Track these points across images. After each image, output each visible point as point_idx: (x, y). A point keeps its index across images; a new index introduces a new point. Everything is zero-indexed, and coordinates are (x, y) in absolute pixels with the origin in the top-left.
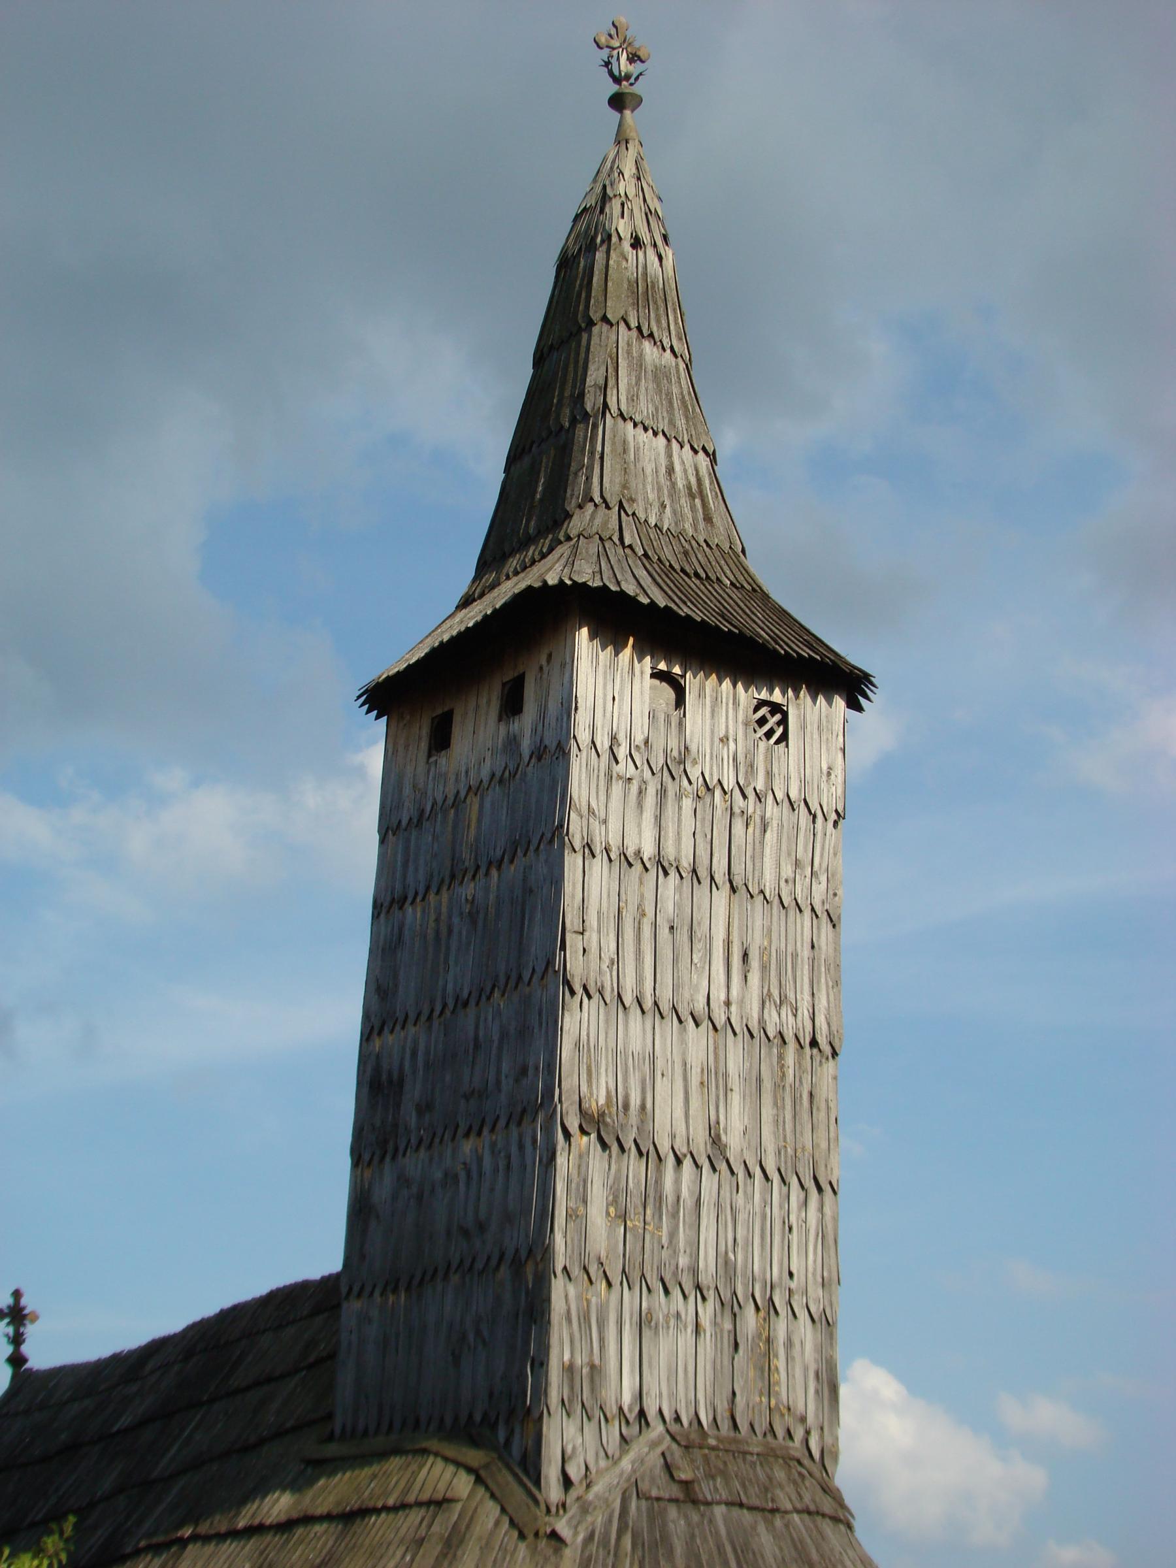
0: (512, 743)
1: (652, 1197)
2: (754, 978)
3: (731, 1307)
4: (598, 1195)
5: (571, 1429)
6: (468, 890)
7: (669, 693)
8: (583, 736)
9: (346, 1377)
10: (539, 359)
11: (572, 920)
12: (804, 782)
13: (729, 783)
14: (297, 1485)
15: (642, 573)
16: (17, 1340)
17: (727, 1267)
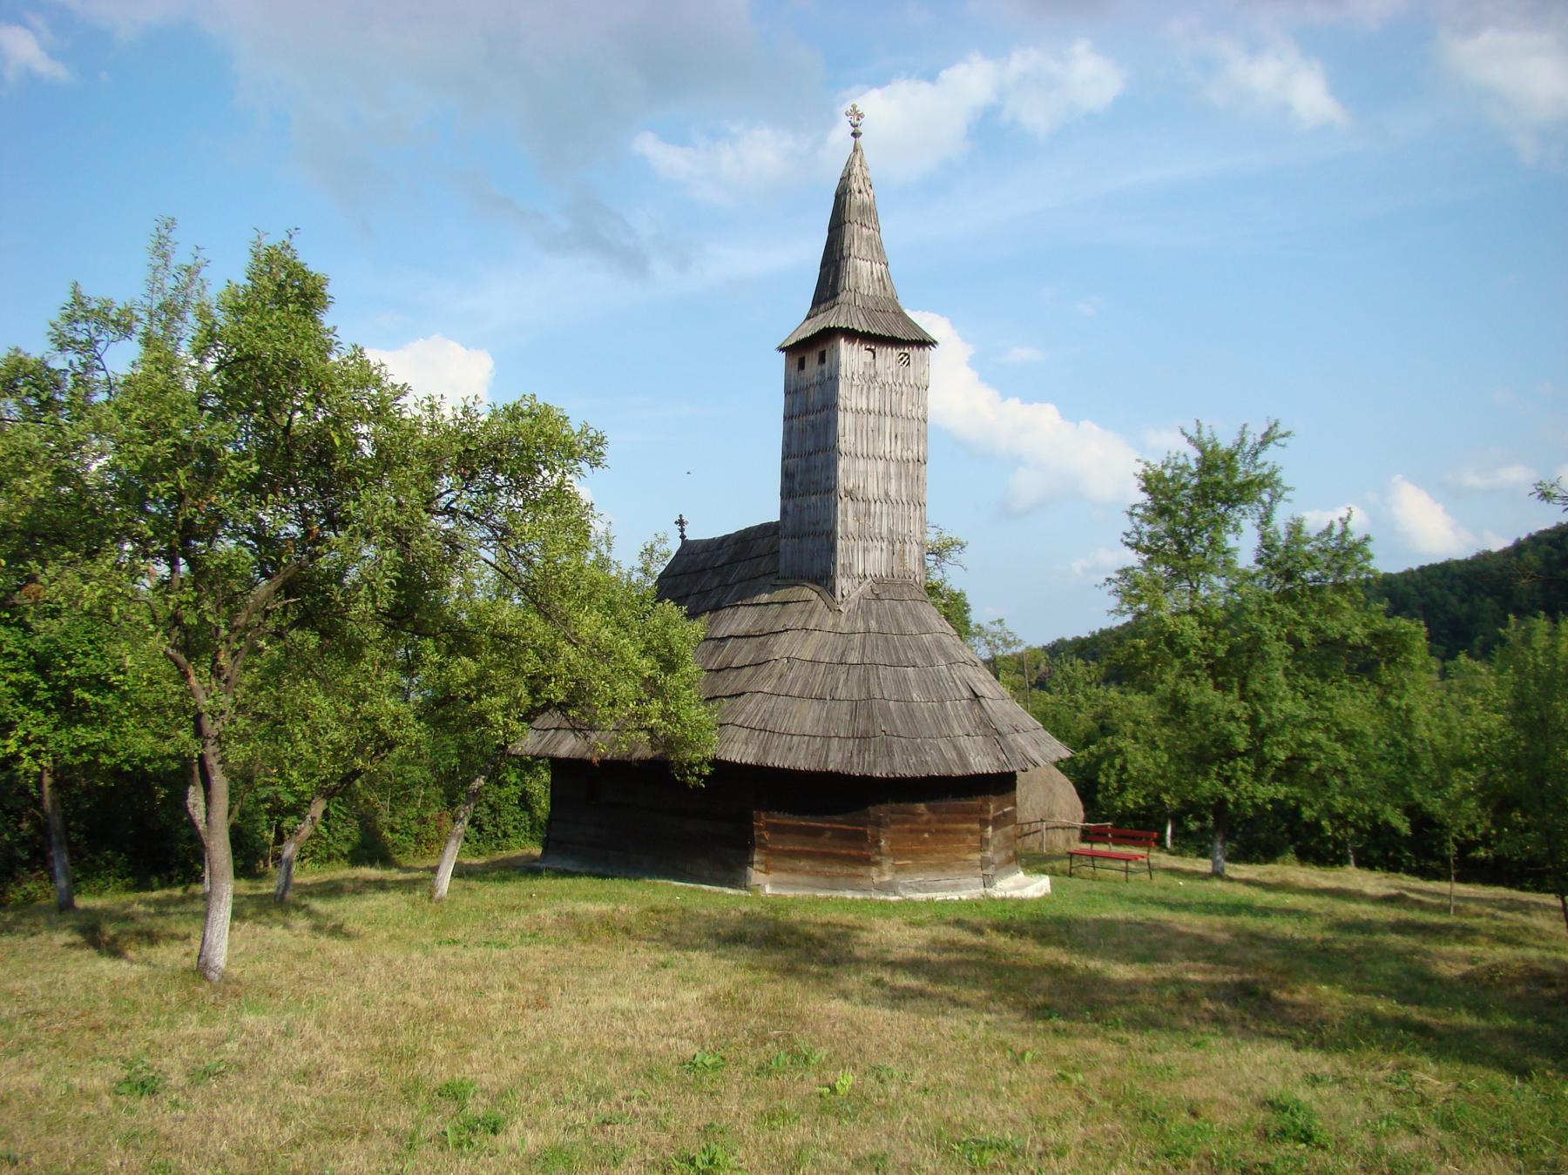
0: (822, 372)
1: (868, 514)
2: (899, 442)
3: (892, 543)
4: (850, 513)
5: (844, 581)
6: (812, 417)
7: (871, 354)
8: (843, 374)
9: (782, 561)
10: (831, 230)
12: (915, 378)
13: (890, 382)
14: (770, 592)
15: (861, 317)
16: (682, 530)
17: (891, 531)
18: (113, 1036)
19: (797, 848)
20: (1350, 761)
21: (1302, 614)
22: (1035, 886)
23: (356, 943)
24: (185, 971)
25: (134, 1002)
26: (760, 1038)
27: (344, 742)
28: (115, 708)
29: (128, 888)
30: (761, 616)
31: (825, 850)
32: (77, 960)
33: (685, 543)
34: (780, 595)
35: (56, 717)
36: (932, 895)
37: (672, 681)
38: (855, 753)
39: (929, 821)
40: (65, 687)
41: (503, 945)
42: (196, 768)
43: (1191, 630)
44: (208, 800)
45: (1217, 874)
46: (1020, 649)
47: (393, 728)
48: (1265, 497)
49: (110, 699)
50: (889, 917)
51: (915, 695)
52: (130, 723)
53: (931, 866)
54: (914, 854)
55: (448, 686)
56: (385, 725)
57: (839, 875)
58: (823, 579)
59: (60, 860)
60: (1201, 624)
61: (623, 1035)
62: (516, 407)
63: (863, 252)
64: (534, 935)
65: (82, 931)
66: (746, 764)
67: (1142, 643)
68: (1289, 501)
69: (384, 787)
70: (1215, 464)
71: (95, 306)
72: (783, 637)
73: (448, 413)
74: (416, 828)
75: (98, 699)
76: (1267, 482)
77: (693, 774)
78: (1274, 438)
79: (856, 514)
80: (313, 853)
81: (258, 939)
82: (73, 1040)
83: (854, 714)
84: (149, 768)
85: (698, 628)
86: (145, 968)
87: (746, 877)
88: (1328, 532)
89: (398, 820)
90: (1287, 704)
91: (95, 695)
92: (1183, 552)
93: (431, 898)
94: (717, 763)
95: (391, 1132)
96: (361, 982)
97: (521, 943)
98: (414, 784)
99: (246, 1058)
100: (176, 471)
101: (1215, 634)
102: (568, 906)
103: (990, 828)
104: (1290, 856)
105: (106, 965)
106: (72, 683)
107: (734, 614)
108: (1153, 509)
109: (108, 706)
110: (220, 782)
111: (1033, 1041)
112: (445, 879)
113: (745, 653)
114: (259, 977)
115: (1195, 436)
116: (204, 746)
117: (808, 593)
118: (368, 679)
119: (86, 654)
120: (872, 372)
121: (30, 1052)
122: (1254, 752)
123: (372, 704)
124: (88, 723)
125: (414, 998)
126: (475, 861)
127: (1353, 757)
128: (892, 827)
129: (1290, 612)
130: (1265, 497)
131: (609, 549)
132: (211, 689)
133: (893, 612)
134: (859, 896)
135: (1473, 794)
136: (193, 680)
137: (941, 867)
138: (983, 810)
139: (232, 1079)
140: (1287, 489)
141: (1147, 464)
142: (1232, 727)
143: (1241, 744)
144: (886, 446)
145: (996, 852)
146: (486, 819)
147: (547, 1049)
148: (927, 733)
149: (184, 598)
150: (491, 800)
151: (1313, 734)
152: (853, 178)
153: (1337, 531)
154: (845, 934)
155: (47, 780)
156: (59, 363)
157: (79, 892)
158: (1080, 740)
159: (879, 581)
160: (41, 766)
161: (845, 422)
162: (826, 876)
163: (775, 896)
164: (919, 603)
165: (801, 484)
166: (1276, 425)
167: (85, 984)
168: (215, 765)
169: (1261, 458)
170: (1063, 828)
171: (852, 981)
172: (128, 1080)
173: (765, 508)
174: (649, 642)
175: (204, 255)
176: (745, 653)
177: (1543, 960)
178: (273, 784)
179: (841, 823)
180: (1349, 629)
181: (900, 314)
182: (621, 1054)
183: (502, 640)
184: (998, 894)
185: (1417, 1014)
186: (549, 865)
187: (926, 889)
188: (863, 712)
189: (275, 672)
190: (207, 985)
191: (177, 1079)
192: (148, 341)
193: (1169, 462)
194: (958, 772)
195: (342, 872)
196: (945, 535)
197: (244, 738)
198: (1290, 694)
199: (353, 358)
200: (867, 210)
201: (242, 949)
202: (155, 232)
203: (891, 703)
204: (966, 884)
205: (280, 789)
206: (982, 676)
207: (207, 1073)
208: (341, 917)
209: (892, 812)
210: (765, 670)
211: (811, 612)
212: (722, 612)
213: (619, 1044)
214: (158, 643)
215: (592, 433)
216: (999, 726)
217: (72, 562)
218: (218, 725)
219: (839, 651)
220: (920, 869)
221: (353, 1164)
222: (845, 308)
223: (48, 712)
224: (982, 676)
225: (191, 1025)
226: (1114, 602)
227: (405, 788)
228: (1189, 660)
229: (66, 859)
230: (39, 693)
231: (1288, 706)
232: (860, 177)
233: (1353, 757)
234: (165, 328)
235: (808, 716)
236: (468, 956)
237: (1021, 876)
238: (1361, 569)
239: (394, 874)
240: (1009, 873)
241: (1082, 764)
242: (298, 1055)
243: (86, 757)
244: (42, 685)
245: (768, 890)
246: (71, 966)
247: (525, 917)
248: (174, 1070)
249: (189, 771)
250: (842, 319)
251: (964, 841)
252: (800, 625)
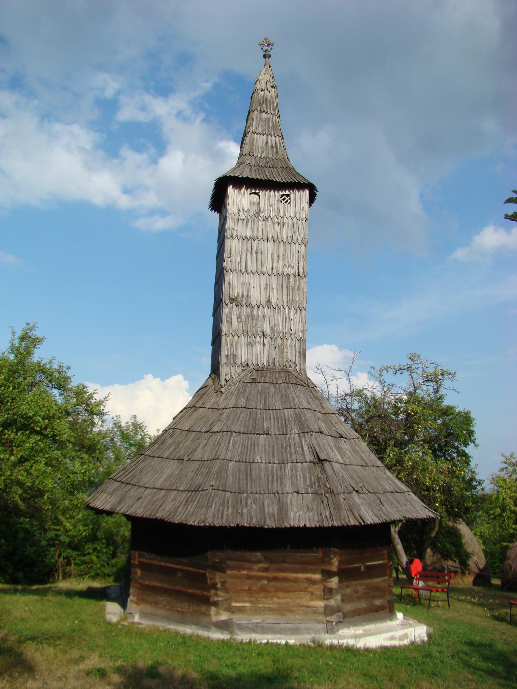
2: (281, 262)
3: (274, 339)
5: (227, 369)
19: (159, 584)
31: (177, 588)
53: (271, 610)
128: (229, 572)
135: (81, 521)
159: (260, 370)
203: (231, 464)
204: (307, 629)
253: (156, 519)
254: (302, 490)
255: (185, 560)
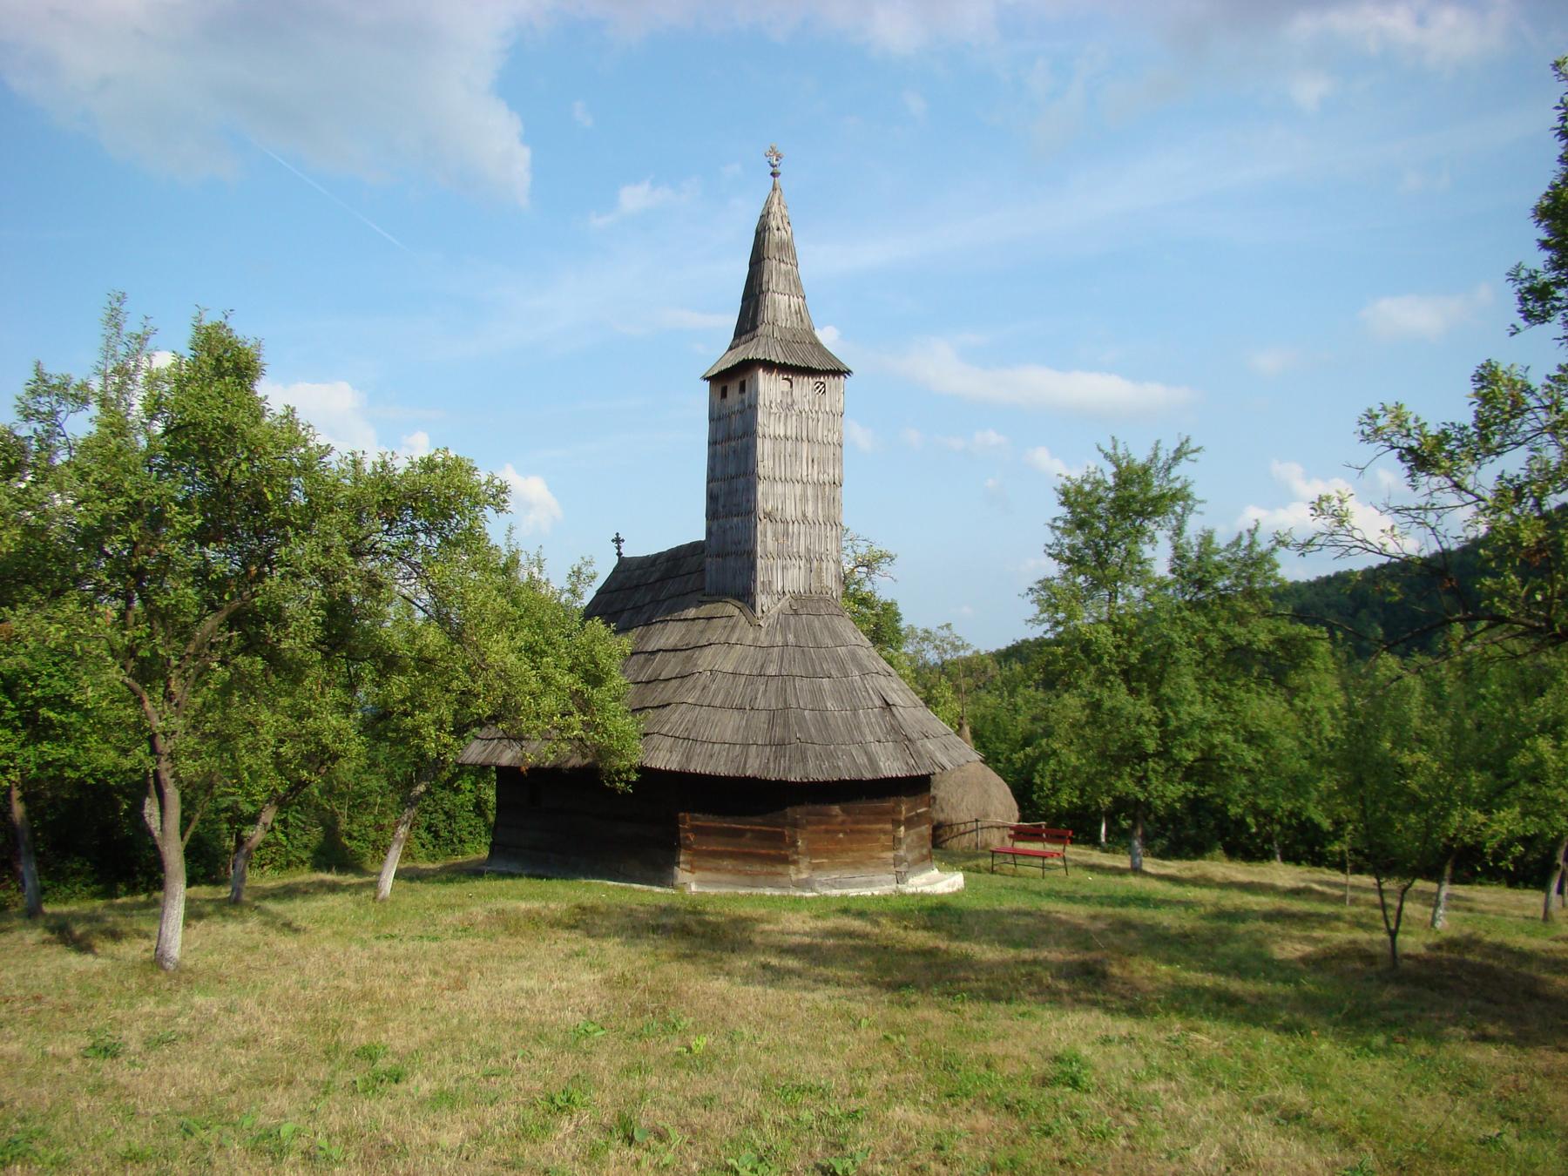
0: (743, 401)
1: (786, 534)
3: (809, 561)
4: (769, 534)
5: (764, 597)
6: (733, 444)
9: (708, 579)
10: (751, 265)
11: (759, 458)
14: (697, 606)
15: (778, 348)
16: (619, 548)
17: (808, 550)
18: (80, 1016)
19: (720, 848)
20: (1258, 761)
21: (1213, 622)
22: (946, 882)
23: (303, 938)
24: (145, 962)
25: (99, 988)
26: (640, 1010)
27: (290, 755)
28: (78, 725)
29: (94, 895)
30: (688, 631)
31: (746, 850)
32: (46, 956)
33: (623, 562)
34: (706, 610)
35: (23, 734)
36: (844, 891)
37: (596, 694)
38: (772, 759)
39: (843, 822)
40: (31, 707)
41: (436, 939)
42: (152, 782)
43: (1105, 638)
44: (162, 808)
45: (1136, 870)
46: (969, 653)
47: (335, 742)
48: (1178, 509)
49: (74, 718)
50: (798, 911)
51: (829, 705)
52: (93, 740)
53: (847, 864)
54: (829, 853)
55: (386, 702)
56: (327, 739)
57: (759, 874)
58: (745, 597)
59: (28, 868)
60: (1114, 633)
61: (522, 1009)
62: (430, 459)
63: (781, 287)
64: (465, 930)
65: (52, 930)
66: (670, 771)
67: (1060, 650)
68: (1201, 513)
69: (342, 795)
70: (1129, 476)
71: (55, 381)
72: (709, 651)
73: (369, 468)
74: (373, 835)
75: (63, 717)
76: (1181, 495)
77: (621, 781)
78: (1185, 454)
79: (775, 534)
80: (272, 860)
81: (212, 936)
82: (45, 1019)
83: (771, 723)
84: (111, 782)
85: (627, 642)
86: (109, 961)
87: (673, 876)
88: (1237, 543)
89: (355, 827)
90: (1196, 708)
91: (59, 714)
92: (1102, 564)
93: (375, 898)
94: (643, 770)
95: (310, 1082)
96: (301, 969)
97: (453, 937)
98: (370, 792)
99: (195, 1029)
100: (128, 526)
101: (1130, 641)
102: (501, 903)
103: (902, 828)
104: (1218, 852)
105: (75, 961)
106: (38, 702)
107: (663, 629)
108: (1071, 523)
109: (71, 724)
110: (173, 794)
111: (871, 1008)
112: (388, 881)
113: (672, 666)
114: (210, 967)
115: (1111, 452)
116: (158, 762)
117: (731, 609)
118: (312, 697)
119: (51, 676)
120: (789, 401)
121: (9, 1029)
122: (1164, 753)
123: (315, 719)
124: (55, 739)
125: (349, 984)
126: (431, 866)
127: (1260, 757)
128: (810, 828)
129: (1201, 620)
130: (1178, 509)
131: (540, 572)
132: (164, 712)
133: (810, 626)
134: (777, 893)
136: (148, 705)
137: (855, 865)
138: (895, 811)
139: (182, 1044)
140: (1200, 502)
141: (1068, 478)
142: (1142, 730)
143: (1151, 746)
144: (803, 470)
145: (909, 849)
146: (441, 825)
147: (455, 1021)
148: (840, 740)
149: (138, 633)
150: (447, 807)
151: (1222, 735)
152: (771, 216)
153: (1245, 542)
154: (740, 923)
155: (16, 794)
156: (25, 431)
157: (46, 901)
158: (1017, 742)
159: (797, 597)
160: (9, 780)
161: (764, 448)
162: (747, 874)
163: (701, 893)
164: (835, 618)
165: (724, 507)
166: (1187, 441)
167: (55, 974)
168: (168, 779)
169: (1174, 473)
170: (998, 828)
171: (742, 963)
172: (94, 1047)
173: (692, 528)
174: (577, 658)
175: (151, 323)
176: (672, 666)
177: (1371, 942)
178: (233, 794)
179: (760, 825)
180: (1255, 636)
181: (817, 345)
182: (517, 1024)
183: (425, 663)
184: (909, 890)
185: (1235, 985)
186: (494, 868)
187: (842, 885)
188: (780, 721)
189: (226, 690)
190: (163, 973)
191: (135, 1045)
192: (104, 402)
193: (1088, 476)
194: (868, 776)
195: (305, 876)
196: (875, 548)
197: (195, 754)
198: (1199, 697)
199: (286, 417)
200: (785, 247)
201: (197, 945)
202: (108, 306)
203: (806, 712)
205: (240, 799)
206: (895, 686)
207: (161, 1041)
208: (290, 916)
209: (809, 814)
210: (689, 682)
211: (733, 628)
212: (652, 627)
213: (517, 1016)
214: (115, 674)
215: (497, 482)
216: (909, 732)
217: (39, 606)
218: (171, 743)
219: (759, 664)
220: (834, 867)
221: (277, 1104)
222: (763, 341)
223: (15, 730)
224: (895, 686)
225: (149, 1005)
226: (1035, 609)
227: (363, 796)
228: (1104, 667)
229: (33, 868)
230: (7, 712)
231: (1197, 709)
232: (778, 216)
233: (1260, 757)
234: (119, 391)
235: (728, 725)
236: (401, 950)
237: (935, 873)
238: (1269, 578)
239: (351, 879)
240: (923, 870)
241: (1018, 765)
242: (239, 1027)
243: (51, 772)
244: (10, 704)
245: (694, 888)
246: (41, 961)
247: (459, 914)
248: (133, 1039)
249: (143, 786)
250: (760, 350)
251: (877, 840)
252: (722, 640)
253: (747, 779)
254: (883, 739)
255: (758, 819)
